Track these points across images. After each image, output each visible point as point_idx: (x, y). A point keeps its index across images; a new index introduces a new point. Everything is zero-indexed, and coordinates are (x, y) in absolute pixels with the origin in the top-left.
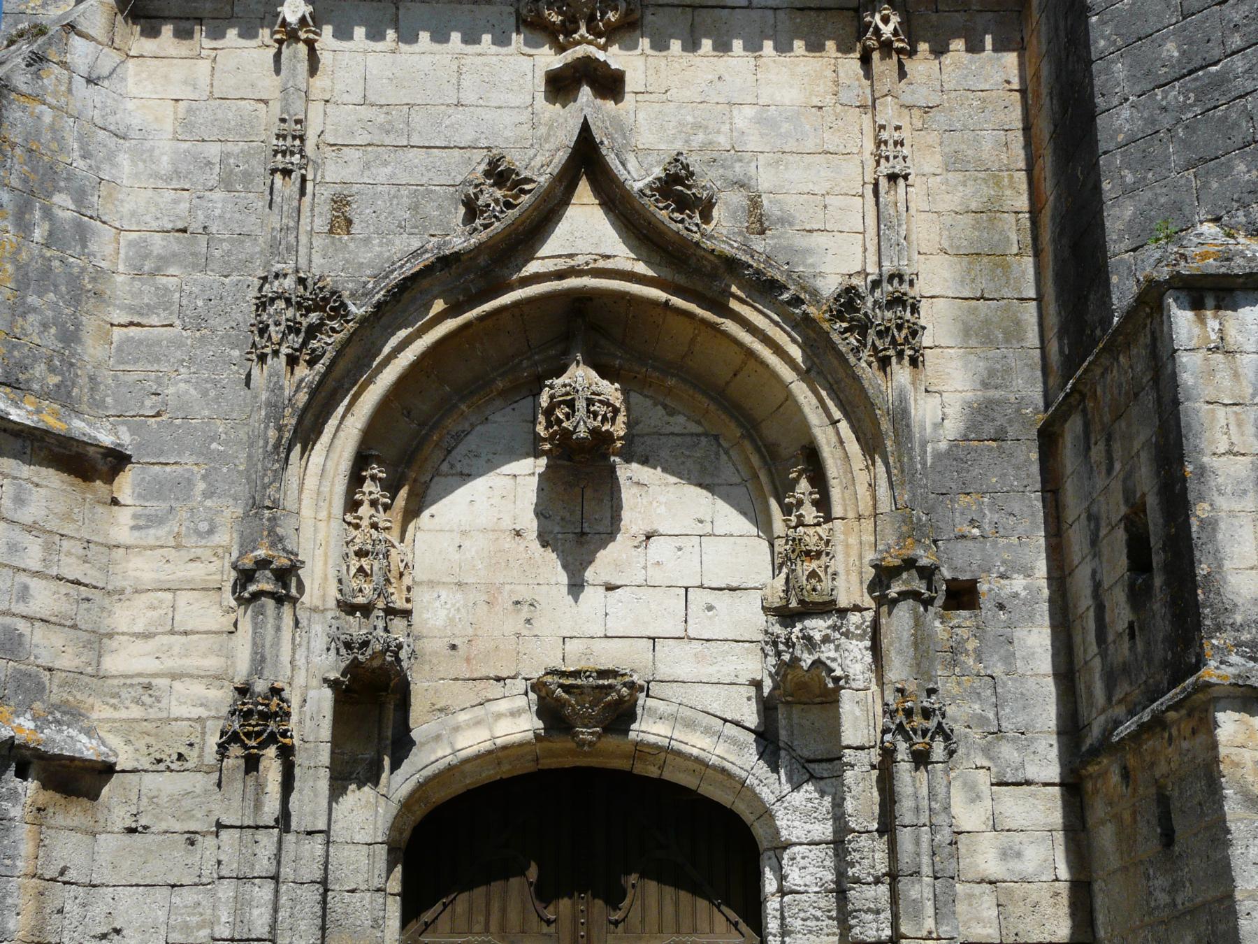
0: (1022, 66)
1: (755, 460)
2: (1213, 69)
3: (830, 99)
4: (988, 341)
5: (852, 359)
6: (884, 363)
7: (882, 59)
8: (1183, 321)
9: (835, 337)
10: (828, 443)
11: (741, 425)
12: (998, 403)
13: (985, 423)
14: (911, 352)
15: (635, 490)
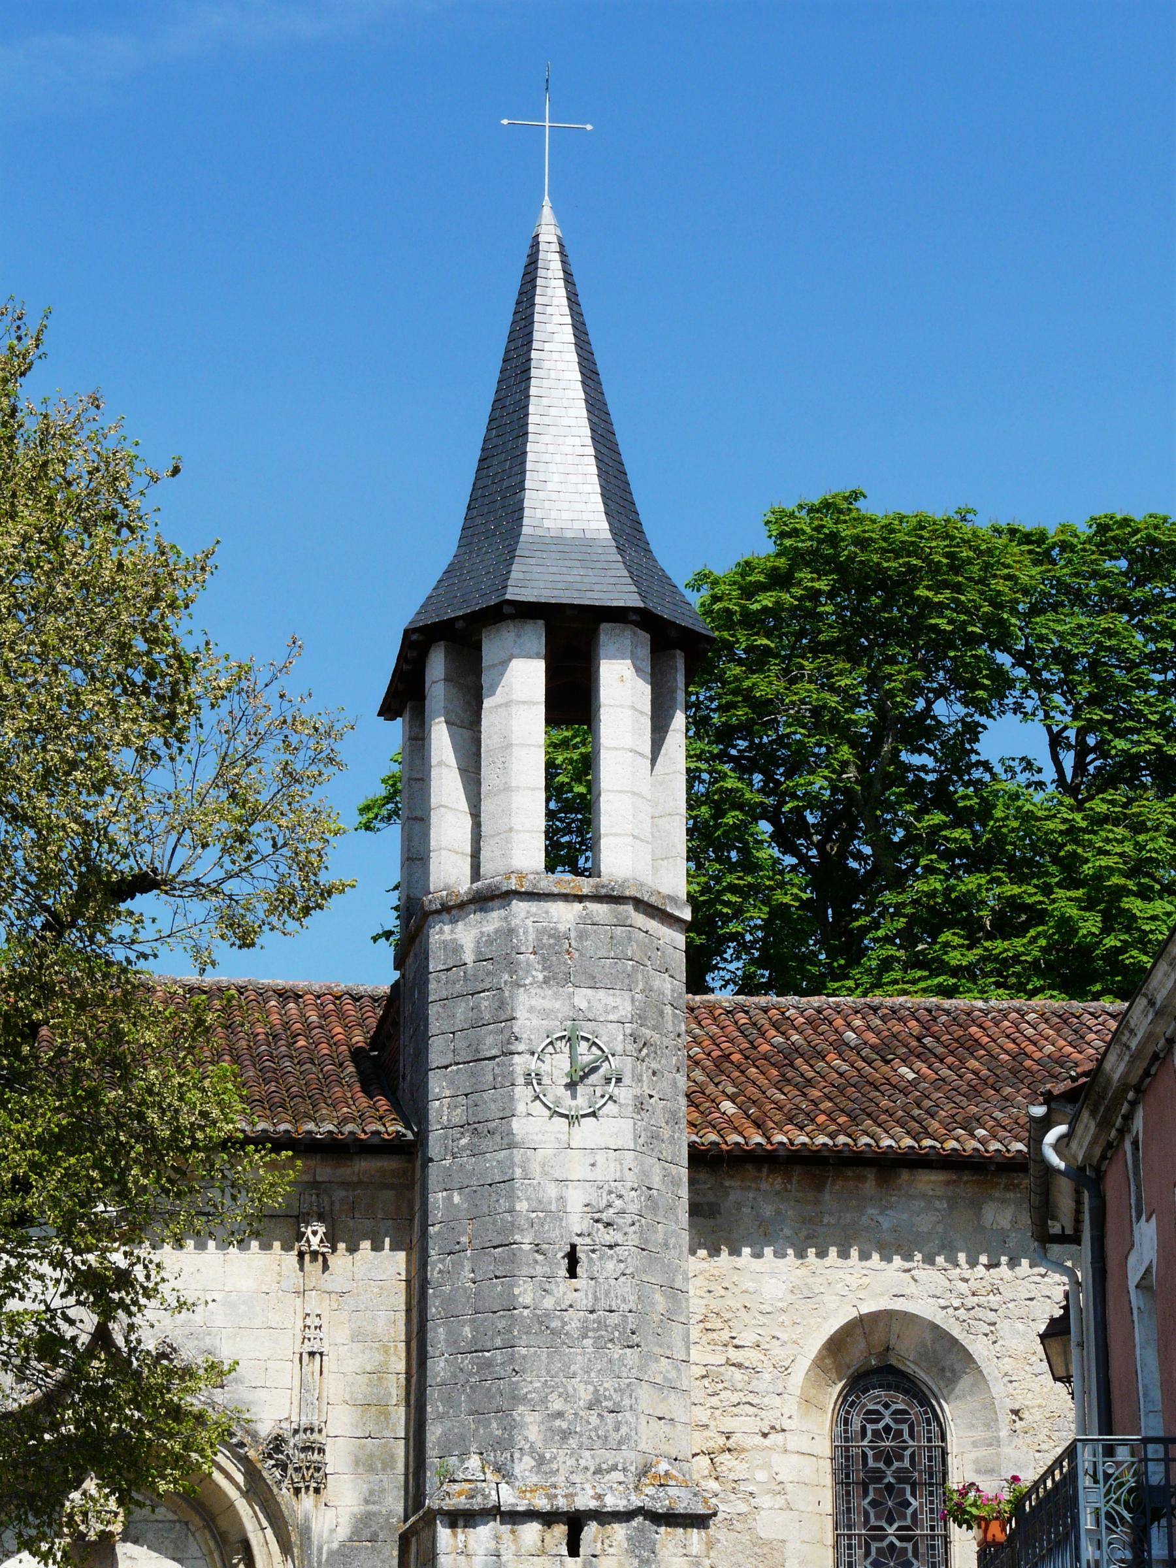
0: (408, 1262)
1: (212, 1543)
2: (487, 1354)
3: (275, 1286)
4: (371, 1469)
5: (275, 1490)
6: (297, 1491)
7: (311, 1262)
8: (444, 1534)
9: (265, 1474)
10: (258, 1543)
11: (204, 1519)
12: (374, 1514)
13: (365, 1528)
14: (315, 1485)
15: (128, 1562)
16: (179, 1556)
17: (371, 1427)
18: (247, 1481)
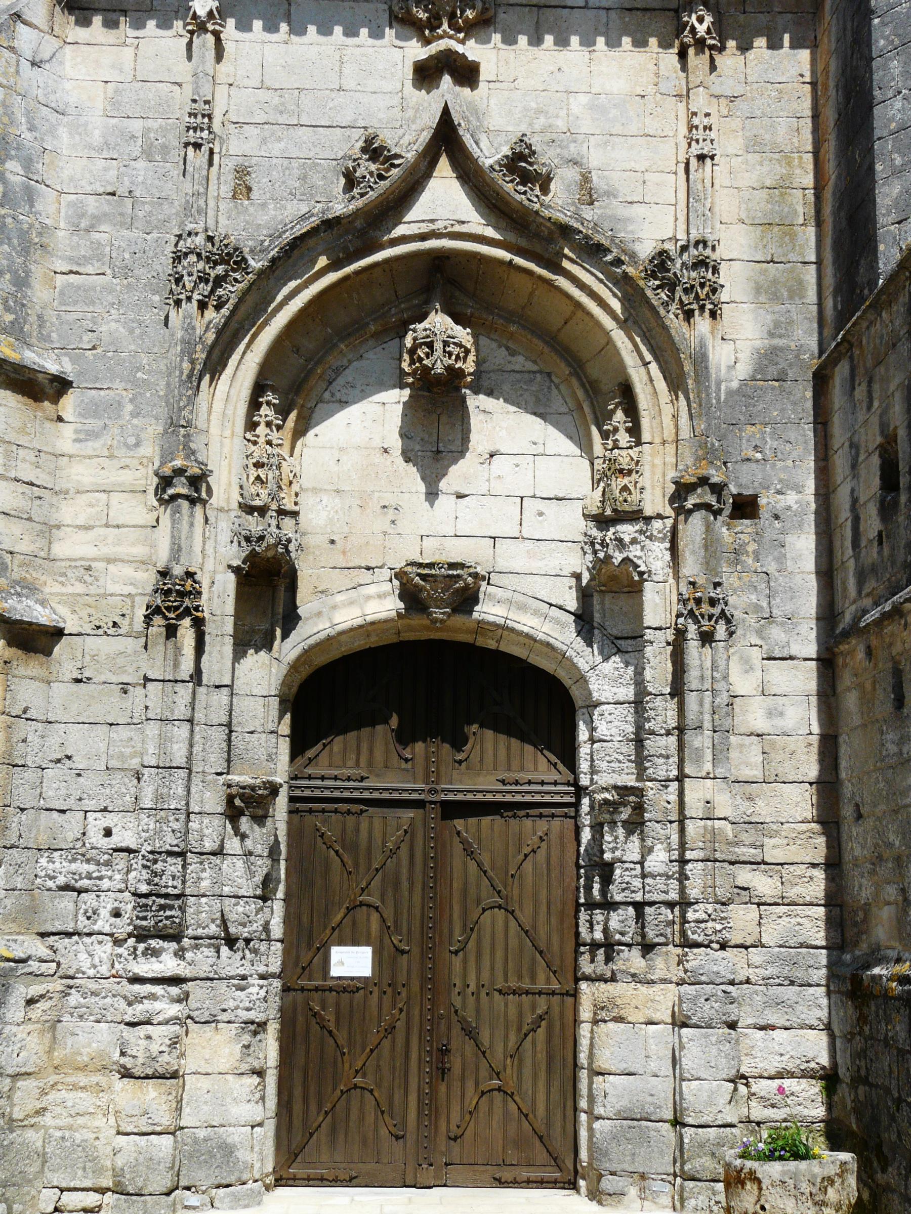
1: (580, 394)
3: (651, 89)
4: (775, 297)
5: (662, 312)
6: (689, 315)
7: (697, 54)
9: (649, 293)
10: (641, 381)
11: (569, 365)
12: (781, 349)
13: (770, 366)
14: (711, 306)
15: (482, 416)
16: (542, 410)
17: (773, 250)
18: (625, 308)
